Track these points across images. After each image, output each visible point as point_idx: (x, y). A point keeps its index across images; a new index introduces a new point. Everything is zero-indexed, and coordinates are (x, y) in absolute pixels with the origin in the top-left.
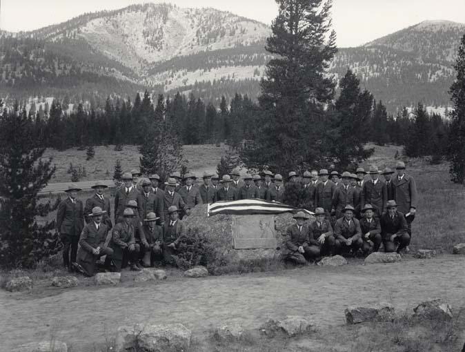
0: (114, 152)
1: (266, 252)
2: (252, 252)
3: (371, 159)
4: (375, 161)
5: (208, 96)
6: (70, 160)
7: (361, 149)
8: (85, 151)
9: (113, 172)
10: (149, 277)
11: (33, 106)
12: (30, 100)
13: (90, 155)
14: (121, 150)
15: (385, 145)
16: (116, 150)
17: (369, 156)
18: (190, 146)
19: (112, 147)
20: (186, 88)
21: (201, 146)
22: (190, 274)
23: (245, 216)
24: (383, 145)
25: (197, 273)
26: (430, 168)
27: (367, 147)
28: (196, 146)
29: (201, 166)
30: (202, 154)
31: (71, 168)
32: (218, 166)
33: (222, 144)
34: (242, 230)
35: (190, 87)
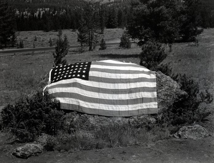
3: (201, 35)
5: (121, 7)
6: (51, 36)
7: (196, 29)
11: (40, 13)
12: (38, 9)
14: (76, 31)
15: (208, 28)
18: (109, 29)
19: (71, 30)
20: (110, 3)
22: (19, 154)
24: (206, 28)
25: (26, 153)
27: (199, 29)
28: (113, 29)
29: (114, 39)
30: (115, 33)
32: (121, 38)
35: (112, 3)
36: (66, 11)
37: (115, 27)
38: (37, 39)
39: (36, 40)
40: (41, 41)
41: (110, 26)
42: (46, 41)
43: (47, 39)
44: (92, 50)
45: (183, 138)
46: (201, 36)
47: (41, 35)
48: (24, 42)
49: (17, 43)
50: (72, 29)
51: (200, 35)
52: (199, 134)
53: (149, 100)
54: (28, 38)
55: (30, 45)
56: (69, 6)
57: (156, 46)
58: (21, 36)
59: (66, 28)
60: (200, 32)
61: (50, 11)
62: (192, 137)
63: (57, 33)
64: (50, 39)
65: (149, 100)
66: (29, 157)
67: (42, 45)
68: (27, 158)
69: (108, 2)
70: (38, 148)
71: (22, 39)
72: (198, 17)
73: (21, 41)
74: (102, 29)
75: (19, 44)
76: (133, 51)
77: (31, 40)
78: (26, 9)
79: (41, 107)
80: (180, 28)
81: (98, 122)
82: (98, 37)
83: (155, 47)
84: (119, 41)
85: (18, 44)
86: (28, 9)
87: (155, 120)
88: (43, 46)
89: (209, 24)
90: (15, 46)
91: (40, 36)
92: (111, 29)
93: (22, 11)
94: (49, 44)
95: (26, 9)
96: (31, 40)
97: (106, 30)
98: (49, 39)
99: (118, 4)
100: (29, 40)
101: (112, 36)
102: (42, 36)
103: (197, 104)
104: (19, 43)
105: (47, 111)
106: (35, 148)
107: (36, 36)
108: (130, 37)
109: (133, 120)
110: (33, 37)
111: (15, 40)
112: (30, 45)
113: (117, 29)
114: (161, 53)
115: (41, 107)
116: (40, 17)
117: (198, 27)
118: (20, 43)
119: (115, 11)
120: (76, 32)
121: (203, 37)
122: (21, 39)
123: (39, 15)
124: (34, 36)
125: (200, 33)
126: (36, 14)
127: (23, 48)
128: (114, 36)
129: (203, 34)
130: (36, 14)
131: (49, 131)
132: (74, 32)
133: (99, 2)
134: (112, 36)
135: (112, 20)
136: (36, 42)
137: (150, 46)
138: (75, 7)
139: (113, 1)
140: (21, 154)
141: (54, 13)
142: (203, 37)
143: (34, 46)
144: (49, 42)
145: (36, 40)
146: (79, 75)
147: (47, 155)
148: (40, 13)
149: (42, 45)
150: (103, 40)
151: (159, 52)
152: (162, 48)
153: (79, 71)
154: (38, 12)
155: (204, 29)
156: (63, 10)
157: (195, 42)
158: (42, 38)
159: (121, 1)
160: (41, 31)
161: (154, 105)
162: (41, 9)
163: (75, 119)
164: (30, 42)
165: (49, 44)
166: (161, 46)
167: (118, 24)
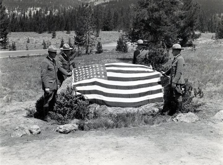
6: (44, 38)
7: (194, 33)
11: (30, 12)
12: (29, 9)
15: (205, 32)
19: (66, 32)
24: (204, 32)
25: (67, 129)
27: (197, 33)
32: (118, 42)
36: (58, 11)
37: (111, 30)
38: (30, 41)
39: (28, 42)
40: (34, 43)
41: (106, 29)
42: (39, 43)
43: (40, 41)
44: (89, 54)
45: (179, 121)
46: (198, 40)
47: (34, 37)
48: (16, 43)
49: (9, 45)
50: (66, 30)
51: (198, 39)
52: (191, 119)
53: (159, 91)
54: (21, 40)
55: (22, 47)
56: (61, 5)
57: (160, 52)
58: (13, 38)
59: (60, 29)
60: (197, 37)
61: (40, 10)
62: (186, 121)
64: (44, 42)
65: (159, 91)
66: (177, 65)
67: (35, 47)
68: (67, 133)
69: (103, 2)
70: (74, 126)
71: (14, 40)
72: (197, 22)
73: (14, 43)
74: (98, 32)
75: (11, 45)
76: (130, 55)
77: (23, 42)
78: (16, 8)
79: (71, 98)
80: (178, 33)
81: (114, 111)
82: (95, 40)
83: (159, 53)
84: (115, 45)
85: (10, 46)
86: (18, 8)
87: (158, 110)
88: (36, 49)
89: (207, 28)
90: (7, 48)
91: (33, 38)
93: (11, 11)
94: (43, 46)
95: (16, 8)
96: (23, 42)
97: (102, 33)
98: (42, 42)
99: (114, 5)
100: (21, 42)
101: (108, 39)
102: (35, 38)
103: (191, 99)
104: (11, 44)
105: (76, 102)
106: (73, 126)
107: (28, 38)
108: (129, 41)
109: (141, 109)
110: (25, 39)
111: (6, 41)
112: (22, 47)
113: (112, 32)
114: (163, 58)
115: (71, 98)
116: (31, 17)
117: (196, 31)
118: (13, 44)
119: (111, 13)
120: (71, 34)
121: (200, 42)
122: (13, 41)
123: (30, 15)
124: (26, 38)
125: (198, 38)
126: (27, 14)
127: (16, 50)
128: (109, 40)
129: (201, 39)
130: (27, 14)
131: (78, 116)
132: (69, 34)
133: (94, 2)
134: (108, 39)
135: (108, 22)
136: (28, 43)
137: (155, 51)
138: (68, 7)
139: (109, 1)
140: (63, 130)
141: (46, 13)
142: (200, 42)
143: (27, 48)
144: (43, 45)
145: (28, 42)
146: (88, 77)
147: (79, 131)
148: (30, 12)
149: (35, 47)
150: (99, 43)
151: (162, 56)
152: (164, 54)
153: (95, 73)
154: (28, 12)
155: (202, 34)
156: (55, 10)
157: (192, 47)
158: (35, 40)
159: (117, 1)
160: (33, 32)
161: (161, 95)
162: (32, 8)
163: (97, 108)
164: (22, 44)
165: (43, 46)
166: (163, 52)
167: (113, 26)
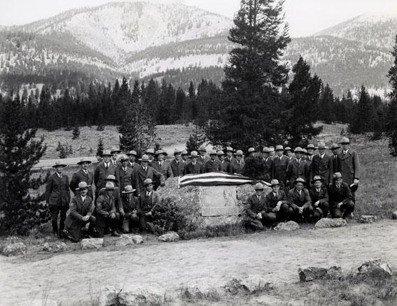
0: (97, 132)
1: (229, 219)
2: (217, 218)
4: (323, 137)
8: (72, 131)
9: (96, 150)
10: (128, 242)
13: (76, 135)
16: (98, 130)
17: (318, 134)
18: (162, 126)
19: (95, 127)
21: (172, 126)
22: (164, 239)
23: (211, 187)
26: (371, 143)
29: (172, 144)
31: (59, 146)
33: (190, 124)
34: (208, 200)
63: (71, 133)
92: (166, 126)
113: (176, 126)
117: (314, 122)
